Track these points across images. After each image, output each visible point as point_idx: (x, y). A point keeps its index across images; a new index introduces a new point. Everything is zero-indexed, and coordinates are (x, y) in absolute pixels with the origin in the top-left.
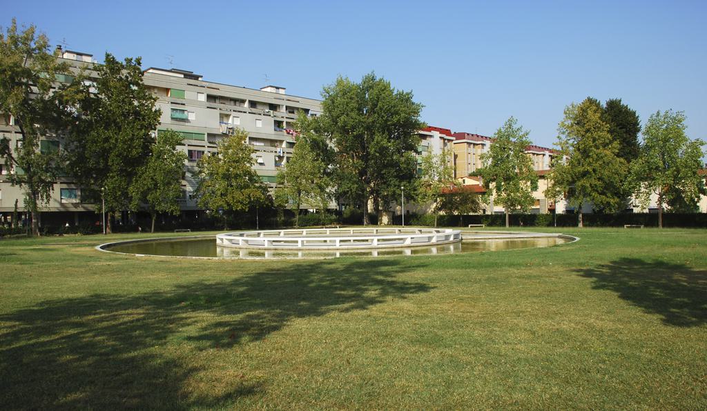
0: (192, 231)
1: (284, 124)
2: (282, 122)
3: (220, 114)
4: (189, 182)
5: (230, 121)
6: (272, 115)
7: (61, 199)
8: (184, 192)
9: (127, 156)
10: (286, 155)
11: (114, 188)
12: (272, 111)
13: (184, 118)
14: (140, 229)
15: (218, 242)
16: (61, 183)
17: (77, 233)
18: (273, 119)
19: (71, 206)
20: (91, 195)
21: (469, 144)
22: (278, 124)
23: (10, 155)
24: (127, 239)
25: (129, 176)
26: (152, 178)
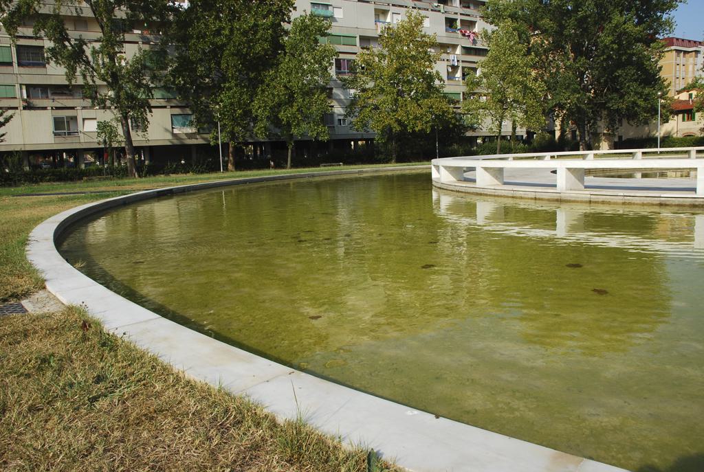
0: (344, 165)
1: (458, 23)
2: (456, 20)
3: (375, 9)
4: (339, 101)
5: (388, 19)
6: (442, 11)
7: (172, 128)
8: (332, 114)
9: (247, 54)
10: (461, 65)
11: (232, 104)
12: (442, 5)
13: (329, 14)
14: (272, 163)
15: (435, 175)
16: (172, 107)
17: (189, 172)
18: (444, 16)
19: (185, 137)
20: (205, 121)
21: (678, 51)
22: (450, 23)
23: (88, 63)
24: (241, 176)
25: (253, 85)
26: (285, 86)
